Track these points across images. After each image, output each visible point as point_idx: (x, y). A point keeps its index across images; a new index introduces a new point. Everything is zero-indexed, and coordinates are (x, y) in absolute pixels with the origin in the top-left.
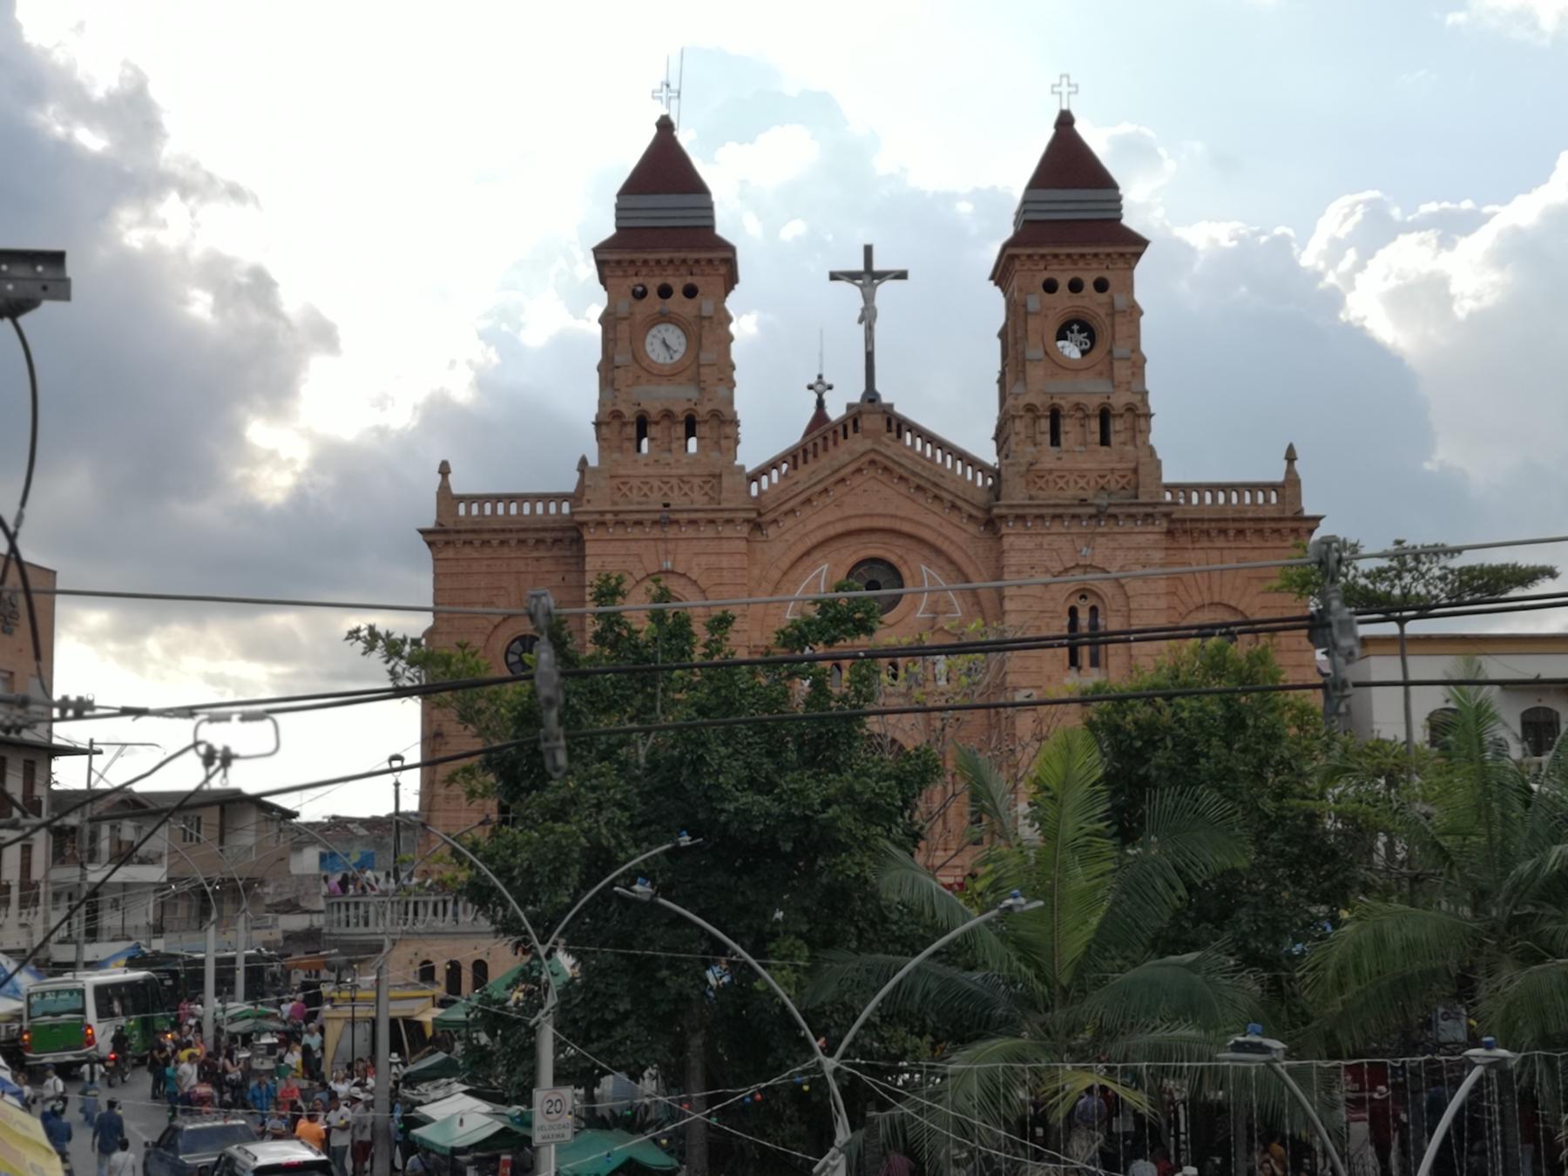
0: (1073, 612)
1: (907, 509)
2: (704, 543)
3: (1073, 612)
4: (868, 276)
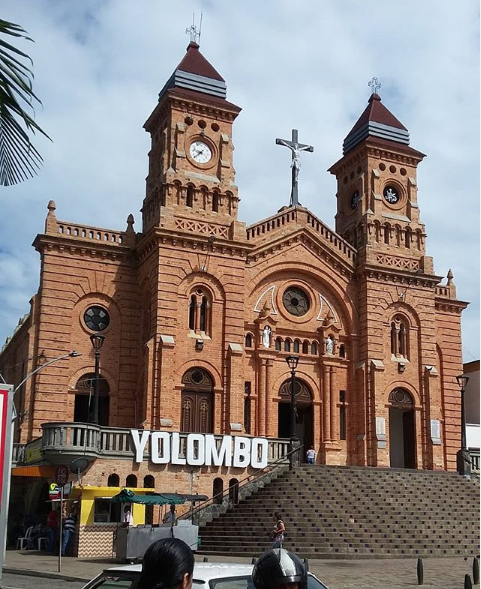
0: (194, 298)
1: (316, 262)
2: (223, 260)
3: (194, 298)
4: (293, 144)
